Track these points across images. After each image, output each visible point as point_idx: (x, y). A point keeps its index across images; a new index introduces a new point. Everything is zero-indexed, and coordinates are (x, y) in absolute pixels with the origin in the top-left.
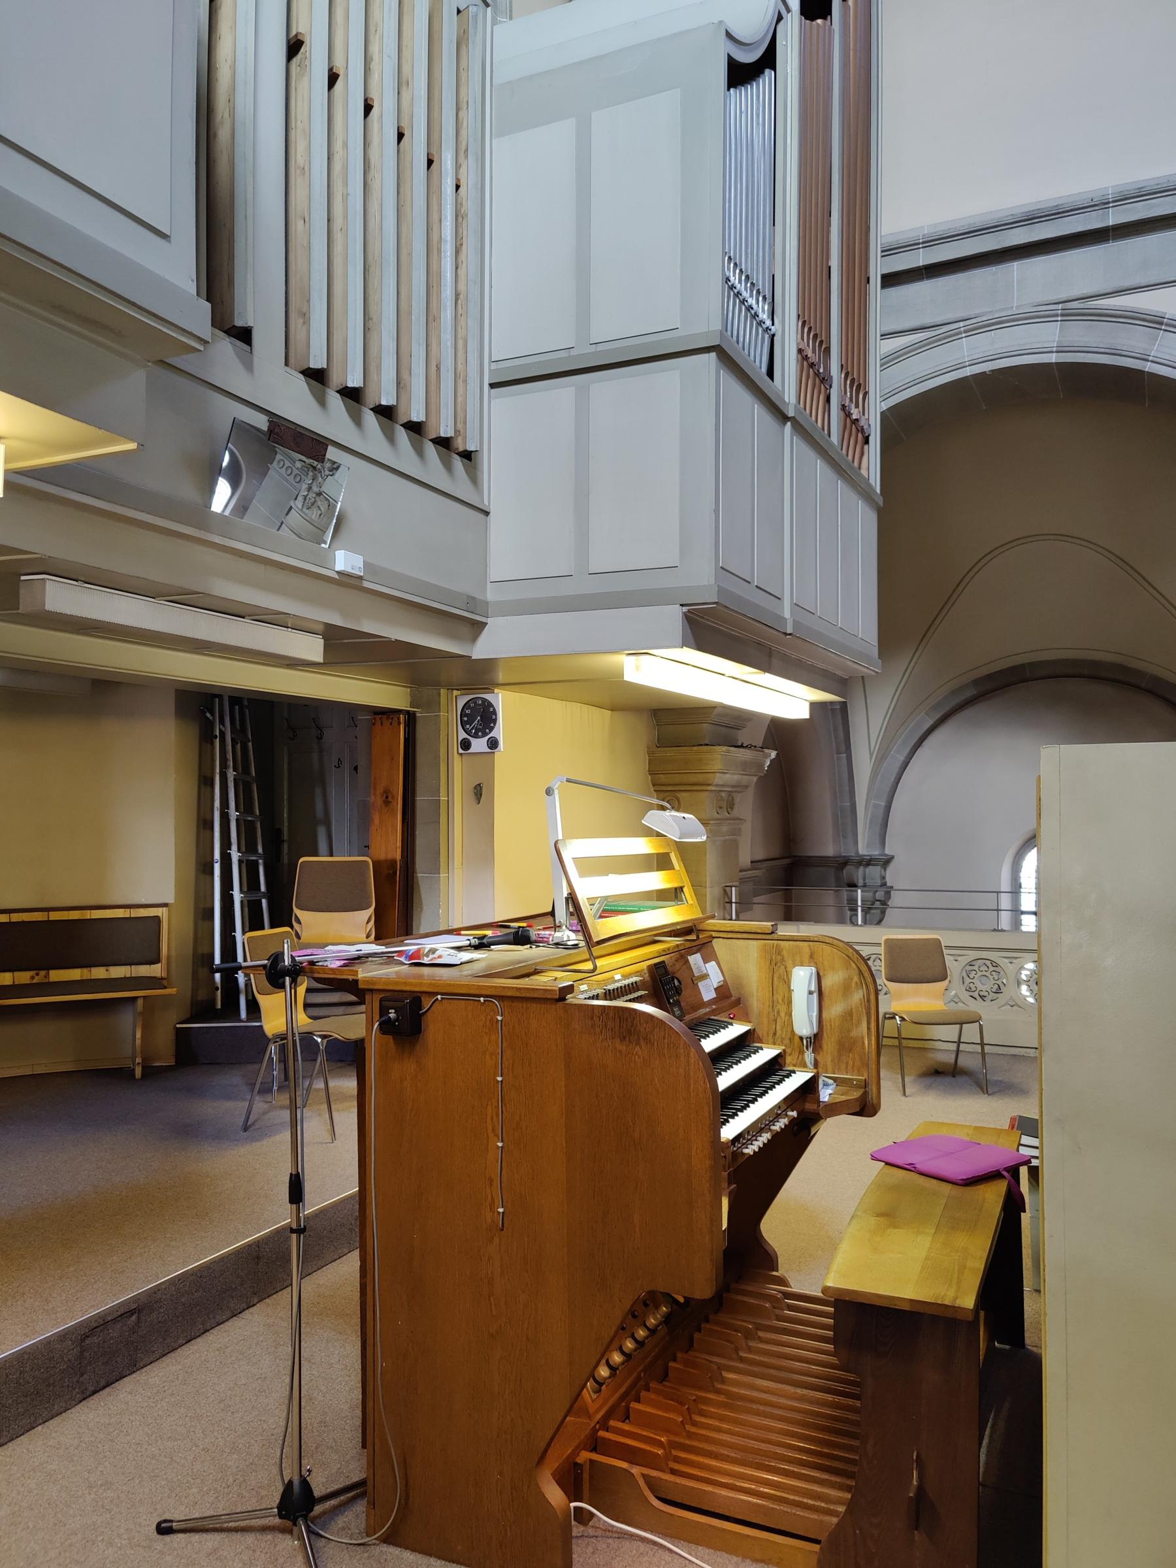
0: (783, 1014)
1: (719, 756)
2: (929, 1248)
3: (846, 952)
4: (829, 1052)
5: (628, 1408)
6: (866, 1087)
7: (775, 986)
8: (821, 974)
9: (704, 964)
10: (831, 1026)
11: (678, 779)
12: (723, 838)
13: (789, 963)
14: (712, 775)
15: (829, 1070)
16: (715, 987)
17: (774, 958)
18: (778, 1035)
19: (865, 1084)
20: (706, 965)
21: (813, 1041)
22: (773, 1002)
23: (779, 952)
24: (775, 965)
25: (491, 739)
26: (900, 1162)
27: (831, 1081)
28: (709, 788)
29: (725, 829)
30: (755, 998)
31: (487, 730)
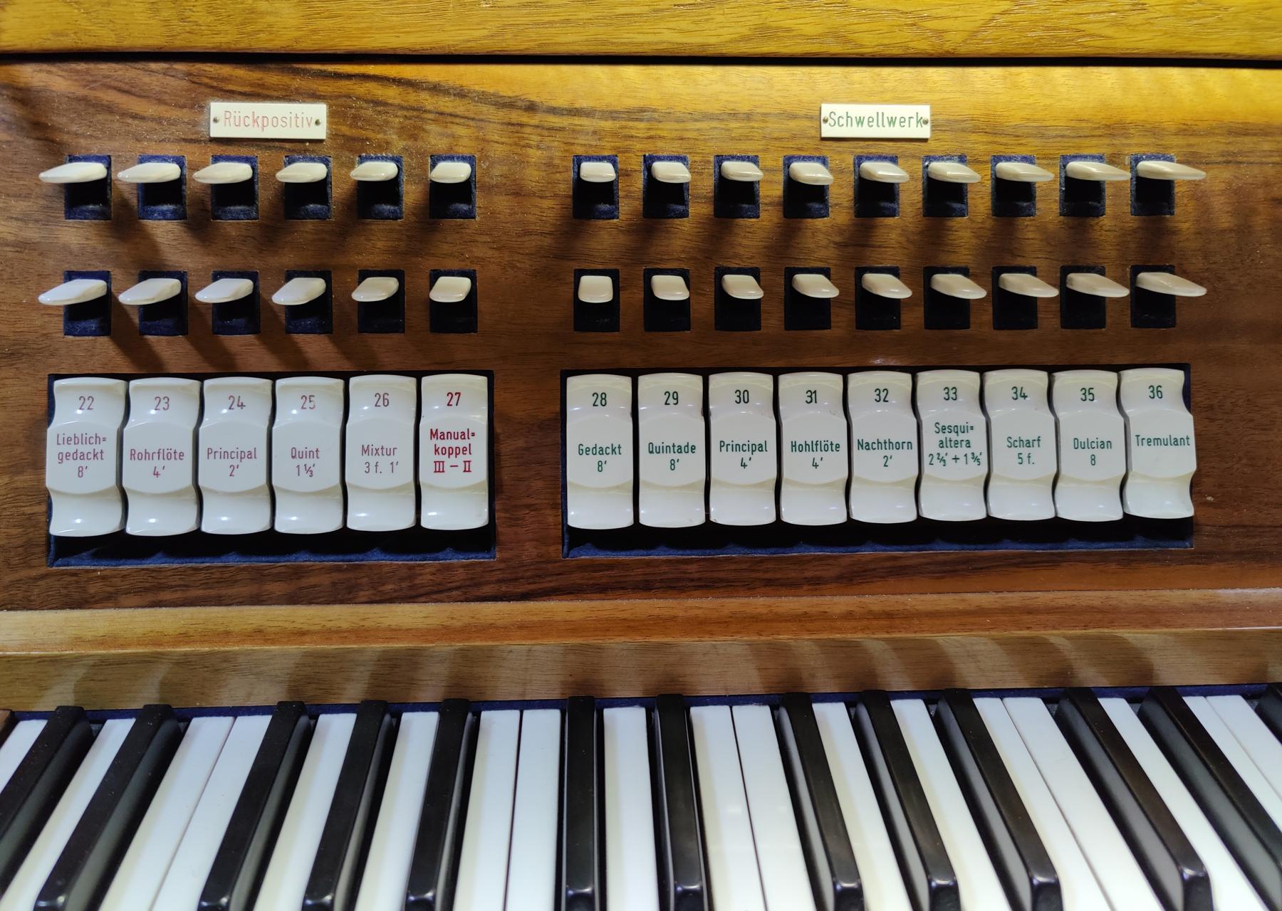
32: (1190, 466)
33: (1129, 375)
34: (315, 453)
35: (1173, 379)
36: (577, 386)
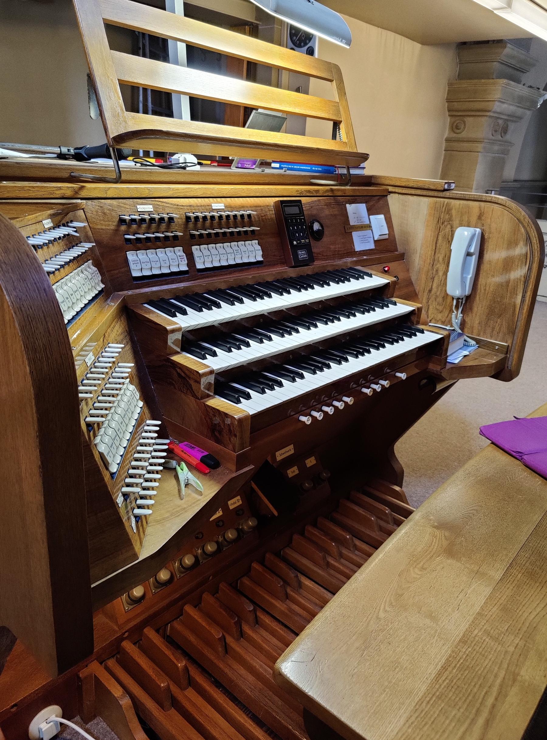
0: (441, 273)
1: (500, 88)
2: (478, 613)
3: (518, 215)
4: (478, 314)
5: (200, 598)
6: (507, 353)
7: (438, 245)
8: (486, 237)
9: (369, 215)
10: (485, 290)
11: (466, 106)
12: (494, 155)
13: (456, 222)
14: (492, 103)
15: (475, 331)
16: (376, 239)
17: (442, 217)
18: (433, 292)
19: (507, 350)
20: (371, 217)
21: (464, 302)
22: (434, 260)
23: (448, 211)
24: (442, 224)
25: (310, 48)
26: (507, 446)
27: (473, 342)
28: (488, 114)
29: (496, 148)
30: (418, 255)
31: (308, 41)
32: (186, 262)
33: (232, 243)
34: (165, 260)
35: (181, 248)
36: (127, 253)
